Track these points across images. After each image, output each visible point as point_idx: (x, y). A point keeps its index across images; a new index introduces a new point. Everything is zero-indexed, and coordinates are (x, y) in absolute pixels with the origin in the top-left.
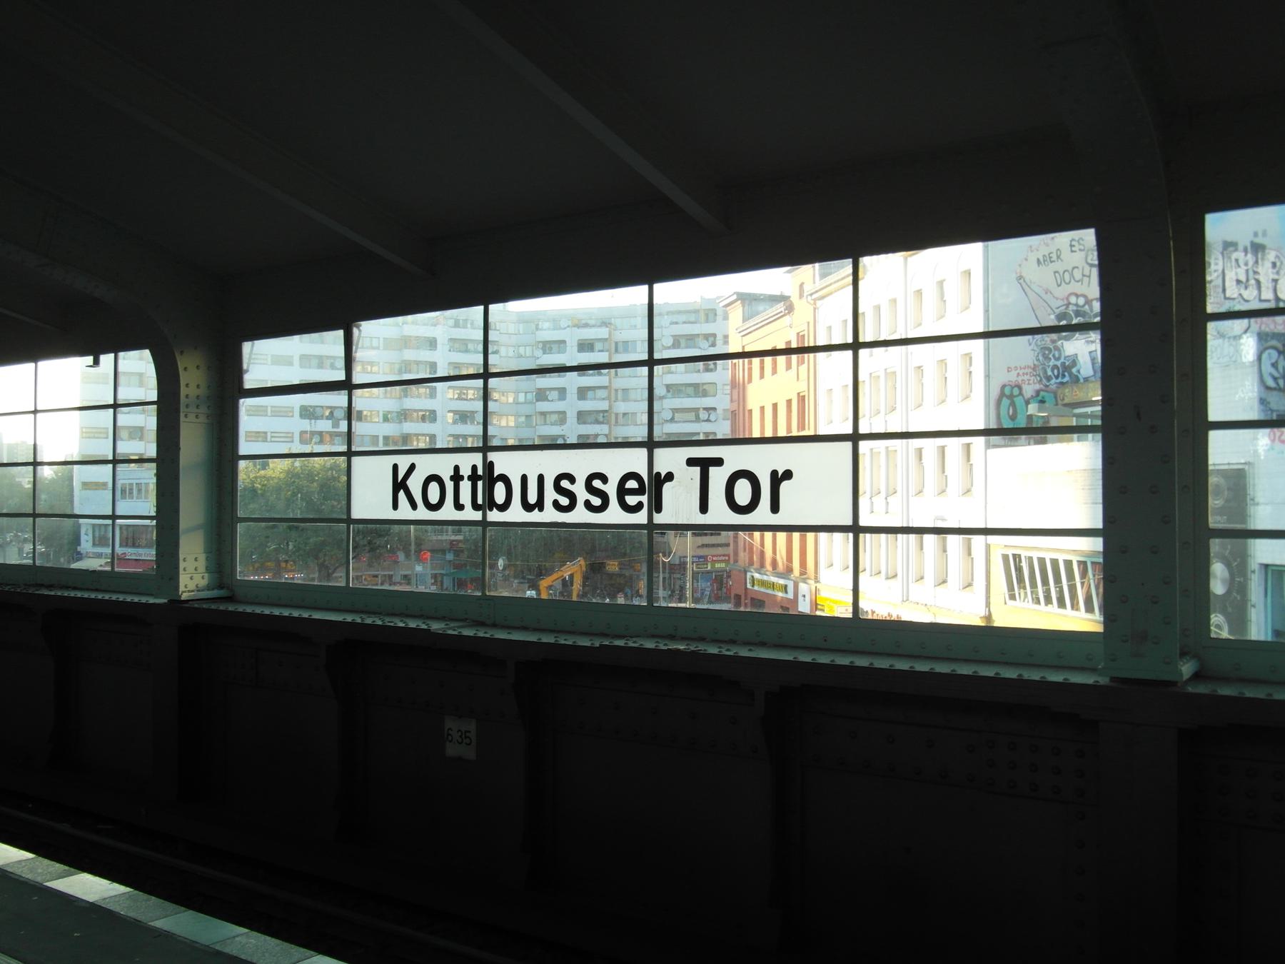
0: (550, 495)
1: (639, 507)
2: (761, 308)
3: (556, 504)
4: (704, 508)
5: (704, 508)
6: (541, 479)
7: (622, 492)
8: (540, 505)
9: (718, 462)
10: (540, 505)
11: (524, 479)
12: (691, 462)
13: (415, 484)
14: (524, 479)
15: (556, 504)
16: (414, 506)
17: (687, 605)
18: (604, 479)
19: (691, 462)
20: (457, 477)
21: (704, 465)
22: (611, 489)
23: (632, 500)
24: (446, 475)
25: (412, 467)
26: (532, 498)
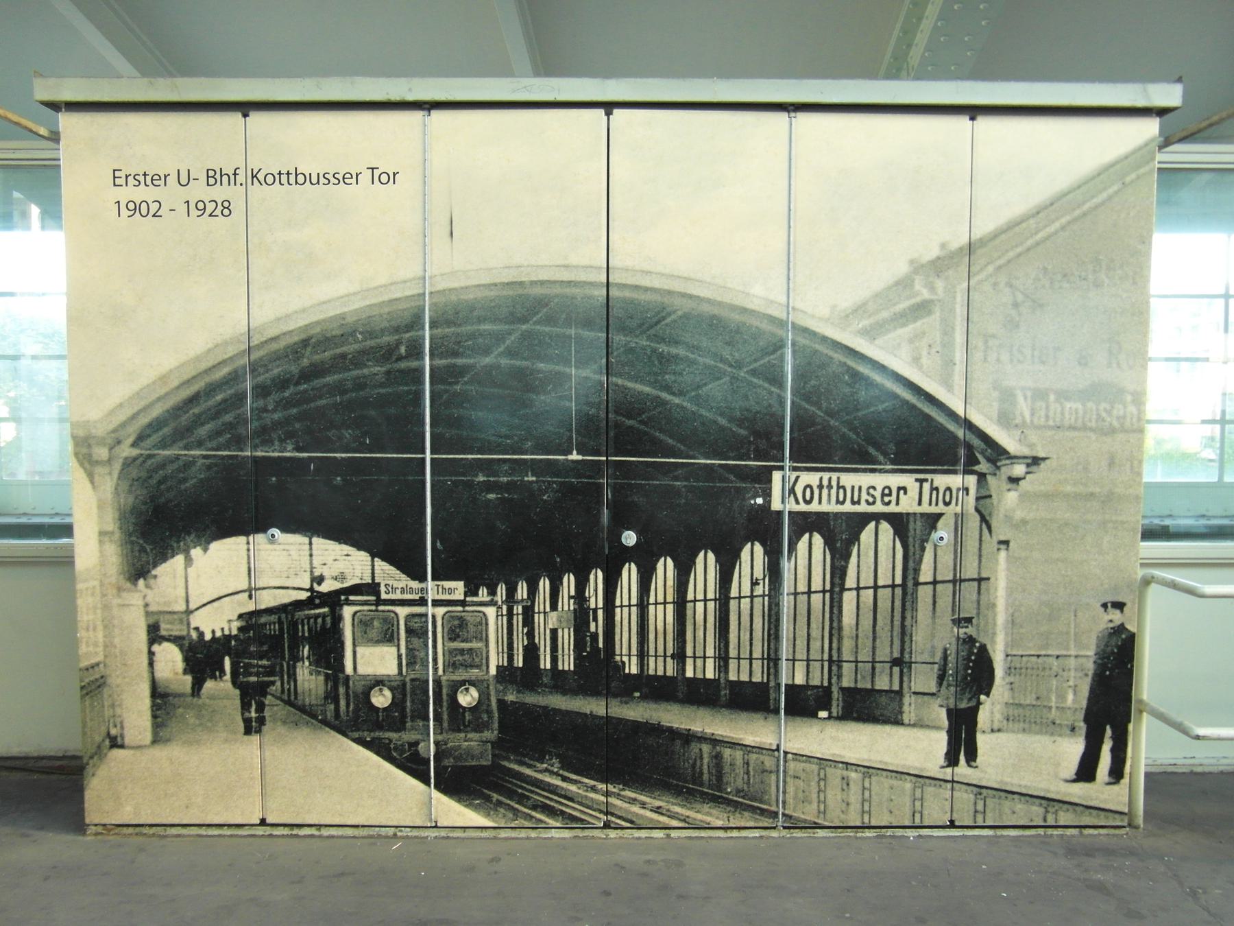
0: (864, 496)
1: (890, 502)
2: (551, 822)
3: (867, 501)
4: (920, 503)
5: (920, 503)
6: (860, 488)
7: (883, 495)
8: (859, 502)
9: (926, 480)
10: (859, 502)
11: (853, 487)
12: (917, 480)
13: (799, 490)
14: (853, 487)
15: (867, 501)
16: (797, 502)
17: (288, 454)
18: (874, 488)
19: (917, 480)
20: (821, 487)
21: (921, 481)
22: (878, 494)
23: (886, 499)
24: (815, 483)
25: (797, 478)
26: (856, 499)
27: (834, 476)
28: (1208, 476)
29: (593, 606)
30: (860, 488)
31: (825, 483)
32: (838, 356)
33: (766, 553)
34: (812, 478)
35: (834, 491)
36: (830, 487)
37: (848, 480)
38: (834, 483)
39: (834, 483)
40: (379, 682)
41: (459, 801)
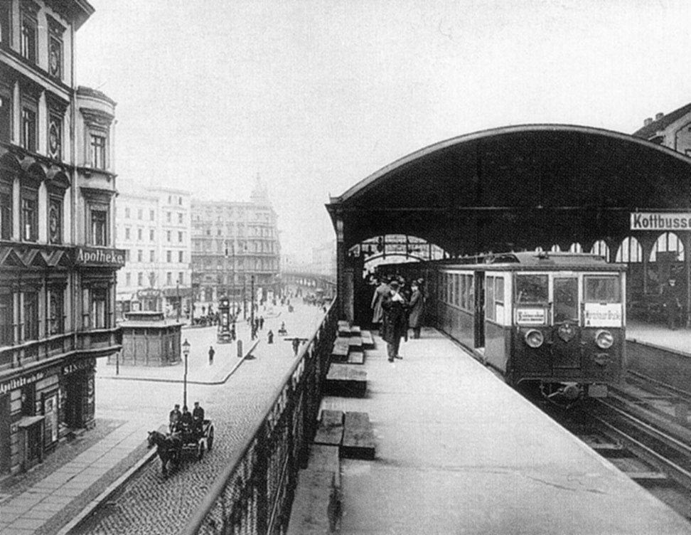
0: (673, 224)
4: (140, 309)
5: (140, 309)
6: (671, 220)
10: (670, 226)
13: (641, 221)
16: (640, 226)
20: (651, 219)
27: (657, 215)
28: (389, 238)
29: (657, 404)
30: (671, 220)
31: (653, 217)
32: (586, 290)
33: (582, 247)
34: (647, 216)
35: (658, 222)
36: (656, 219)
37: (663, 216)
38: (657, 217)
39: (657, 217)
40: (445, 256)
41: (581, 438)
